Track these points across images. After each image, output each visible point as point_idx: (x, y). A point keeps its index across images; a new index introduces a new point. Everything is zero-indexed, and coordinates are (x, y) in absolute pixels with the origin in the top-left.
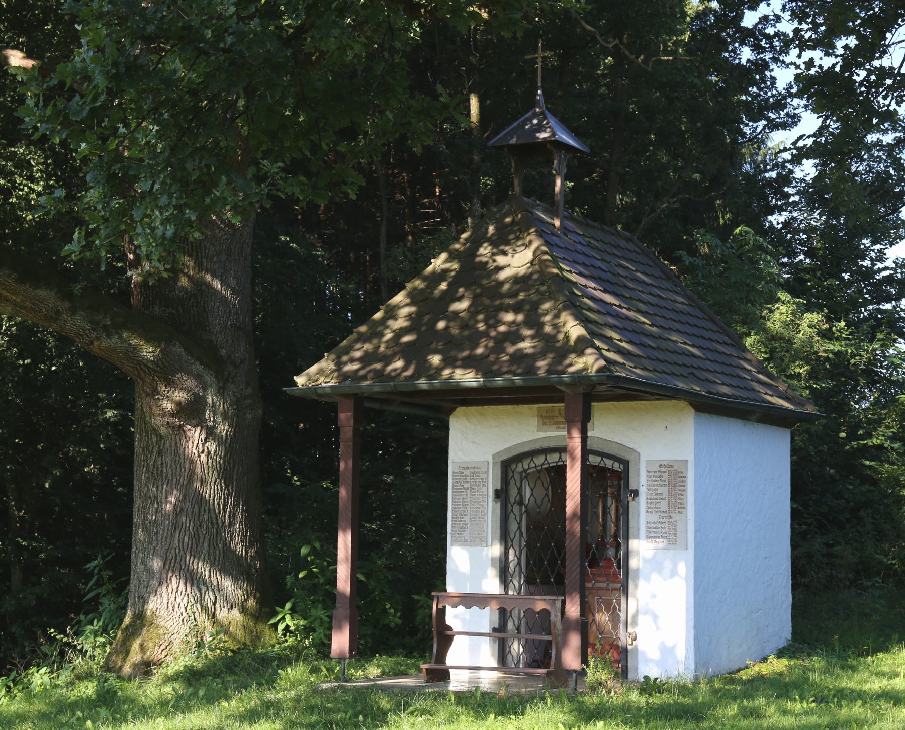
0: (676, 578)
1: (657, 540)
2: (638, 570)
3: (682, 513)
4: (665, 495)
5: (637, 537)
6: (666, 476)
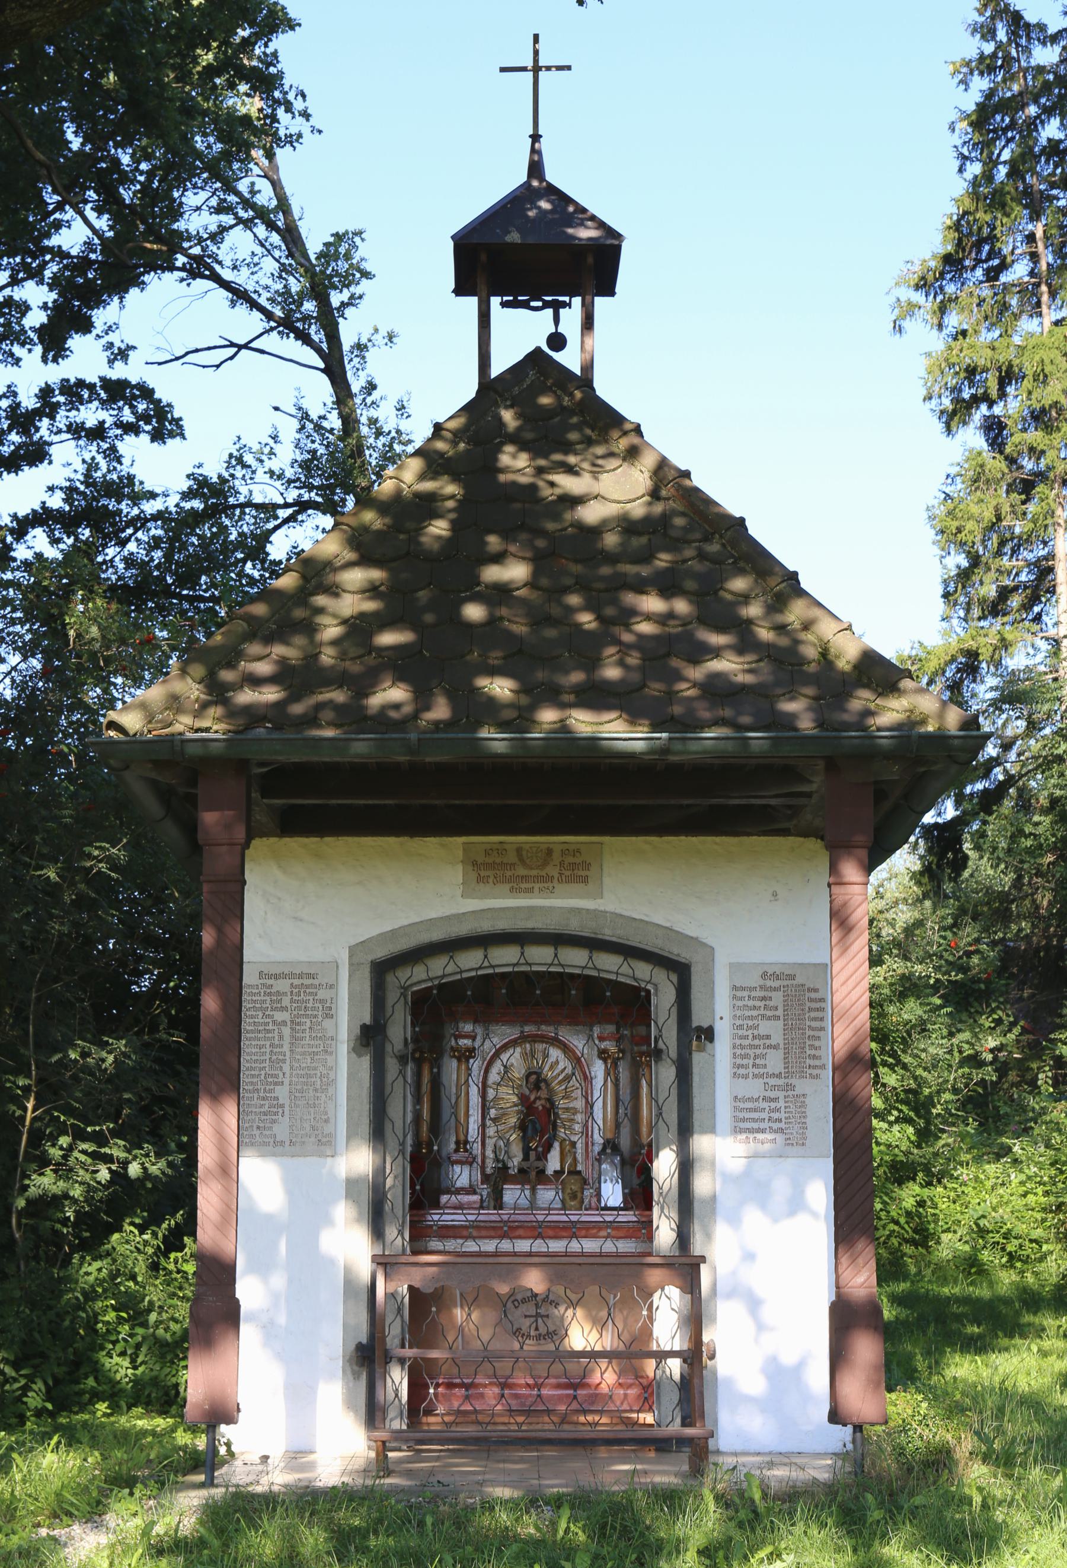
0: (802, 1218)
1: (760, 1136)
2: (714, 1198)
3: (817, 1076)
4: (777, 1038)
5: (712, 1130)
6: (777, 998)
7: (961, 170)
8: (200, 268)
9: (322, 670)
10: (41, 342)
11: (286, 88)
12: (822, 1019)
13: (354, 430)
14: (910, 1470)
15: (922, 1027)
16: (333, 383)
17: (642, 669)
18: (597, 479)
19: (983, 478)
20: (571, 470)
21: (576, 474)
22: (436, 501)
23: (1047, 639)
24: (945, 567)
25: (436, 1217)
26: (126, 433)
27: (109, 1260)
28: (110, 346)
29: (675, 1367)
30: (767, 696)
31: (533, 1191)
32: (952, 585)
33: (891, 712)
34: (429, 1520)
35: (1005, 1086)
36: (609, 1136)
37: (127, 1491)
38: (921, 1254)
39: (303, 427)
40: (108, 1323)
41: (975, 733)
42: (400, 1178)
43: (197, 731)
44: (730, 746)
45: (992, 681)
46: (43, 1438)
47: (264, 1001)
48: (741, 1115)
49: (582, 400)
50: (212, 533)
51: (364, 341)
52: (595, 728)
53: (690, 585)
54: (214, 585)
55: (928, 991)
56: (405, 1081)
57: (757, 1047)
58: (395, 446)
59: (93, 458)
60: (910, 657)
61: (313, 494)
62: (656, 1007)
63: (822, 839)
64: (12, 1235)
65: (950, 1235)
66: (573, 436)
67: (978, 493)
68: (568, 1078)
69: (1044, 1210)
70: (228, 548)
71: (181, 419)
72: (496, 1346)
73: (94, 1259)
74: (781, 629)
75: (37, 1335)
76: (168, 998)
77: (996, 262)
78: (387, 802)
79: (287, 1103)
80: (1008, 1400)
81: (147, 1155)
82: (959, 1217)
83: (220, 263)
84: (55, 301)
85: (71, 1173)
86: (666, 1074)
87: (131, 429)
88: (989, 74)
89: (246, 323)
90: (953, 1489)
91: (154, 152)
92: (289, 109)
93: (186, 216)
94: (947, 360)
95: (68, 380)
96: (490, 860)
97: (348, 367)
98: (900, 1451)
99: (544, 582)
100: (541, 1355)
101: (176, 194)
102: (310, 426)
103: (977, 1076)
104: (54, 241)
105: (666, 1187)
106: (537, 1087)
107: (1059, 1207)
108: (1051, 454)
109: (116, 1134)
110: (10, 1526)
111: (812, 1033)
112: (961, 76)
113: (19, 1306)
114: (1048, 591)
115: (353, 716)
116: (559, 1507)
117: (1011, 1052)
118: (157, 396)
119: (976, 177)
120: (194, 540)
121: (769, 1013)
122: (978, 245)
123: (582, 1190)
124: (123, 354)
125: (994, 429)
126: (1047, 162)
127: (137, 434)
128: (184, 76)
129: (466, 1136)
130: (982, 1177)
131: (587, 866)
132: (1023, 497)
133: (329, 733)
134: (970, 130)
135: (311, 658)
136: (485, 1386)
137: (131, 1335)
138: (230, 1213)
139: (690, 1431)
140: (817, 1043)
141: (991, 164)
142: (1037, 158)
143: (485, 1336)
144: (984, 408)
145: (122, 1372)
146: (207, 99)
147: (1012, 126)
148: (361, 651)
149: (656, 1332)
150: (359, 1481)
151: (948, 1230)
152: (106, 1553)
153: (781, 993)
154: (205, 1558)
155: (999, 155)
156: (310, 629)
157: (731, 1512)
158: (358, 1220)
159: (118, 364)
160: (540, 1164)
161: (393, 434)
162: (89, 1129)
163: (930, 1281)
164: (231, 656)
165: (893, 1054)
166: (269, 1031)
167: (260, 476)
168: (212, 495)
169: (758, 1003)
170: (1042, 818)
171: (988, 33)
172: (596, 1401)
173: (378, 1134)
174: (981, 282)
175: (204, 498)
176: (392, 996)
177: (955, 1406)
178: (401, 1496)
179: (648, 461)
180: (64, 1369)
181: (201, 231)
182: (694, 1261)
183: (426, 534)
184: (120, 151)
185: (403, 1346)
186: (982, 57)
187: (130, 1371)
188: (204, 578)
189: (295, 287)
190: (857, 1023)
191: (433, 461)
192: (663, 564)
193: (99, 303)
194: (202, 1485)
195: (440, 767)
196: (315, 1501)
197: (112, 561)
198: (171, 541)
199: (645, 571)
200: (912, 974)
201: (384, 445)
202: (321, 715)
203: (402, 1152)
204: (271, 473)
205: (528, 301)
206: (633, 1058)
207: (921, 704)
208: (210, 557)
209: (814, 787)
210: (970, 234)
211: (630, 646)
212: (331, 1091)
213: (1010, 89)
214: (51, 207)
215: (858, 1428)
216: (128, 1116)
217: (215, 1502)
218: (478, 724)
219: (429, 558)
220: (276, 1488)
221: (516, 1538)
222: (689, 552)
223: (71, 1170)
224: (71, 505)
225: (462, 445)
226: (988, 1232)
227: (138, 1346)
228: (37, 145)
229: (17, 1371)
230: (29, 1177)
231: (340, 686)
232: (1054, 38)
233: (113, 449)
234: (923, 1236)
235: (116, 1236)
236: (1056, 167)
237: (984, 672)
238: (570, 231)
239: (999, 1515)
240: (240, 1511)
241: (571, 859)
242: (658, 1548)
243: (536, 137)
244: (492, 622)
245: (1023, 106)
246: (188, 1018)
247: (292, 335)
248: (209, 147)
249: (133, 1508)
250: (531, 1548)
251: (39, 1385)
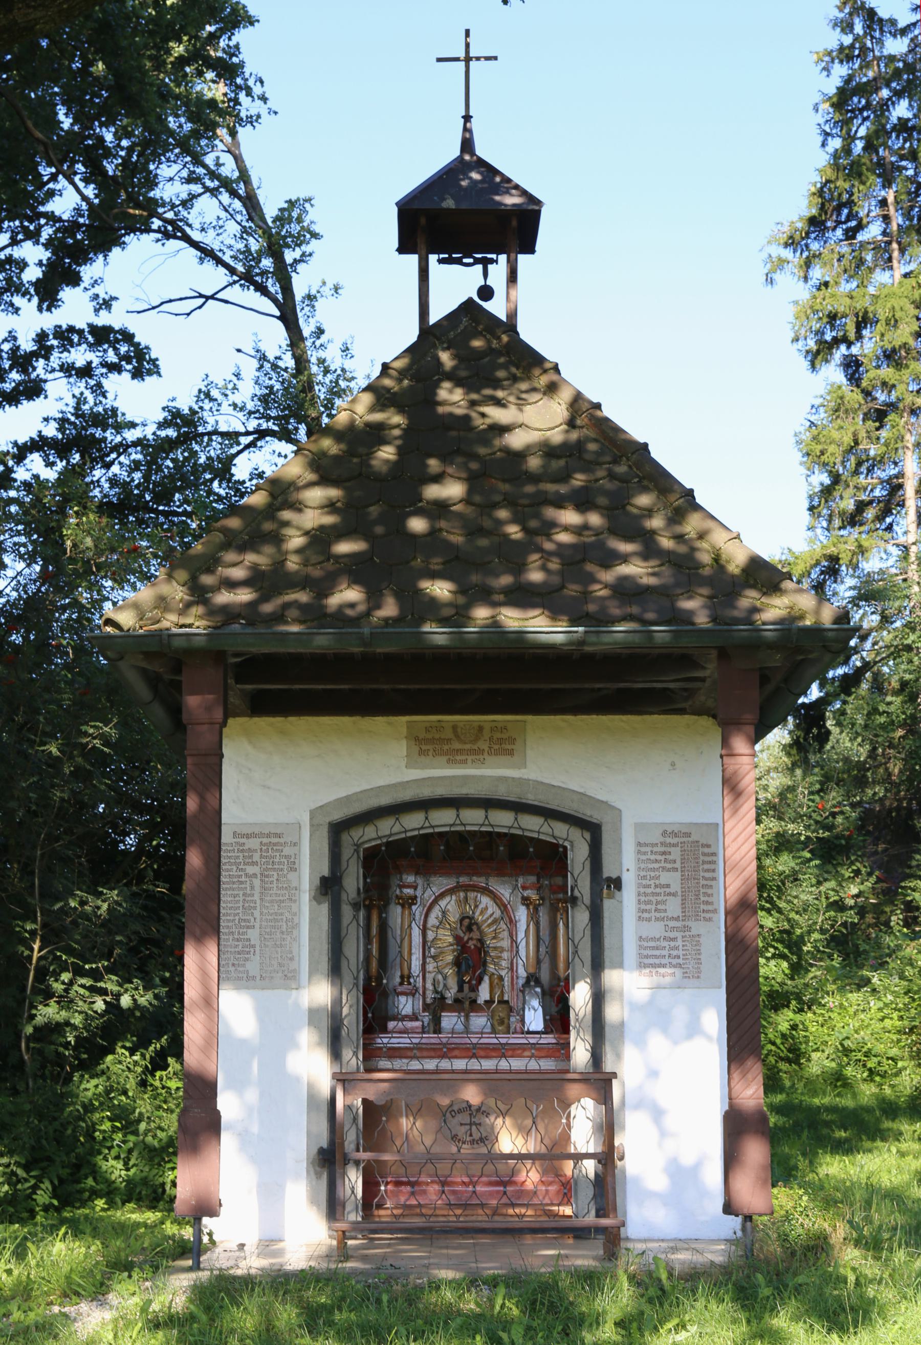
0: (698, 1043)
1: (662, 970)
2: (622, 1024)
3: (710, 919)
4: (676, 887)
5: (620, 965)
6: (676, 853)
7: (824, 145)
8: (175, 231)
9: (288, 574)
10: (37, 293)
11: (247, 75)
12: (714, 871)
13: (305, 369)
14: (793, 1254)
15: (794, 877)
16: (288, 328)
17: (561, 573)
18: (521, 410)
19: (843, 409)
20: (499, 403)
21: (504, 406)
22: (384, 429)
23: (898, 545)
24: (810, 484)
25: (385, 1041)
26: (110, 372)
27: (104, 1078)
28: (96, 296)
29: (590, 1167)
30: (668, 596)
31: (467, 1017)
32: (817, 499)
33: (774, 609)
34: (385, 1298)
35: (863, 927)
36: (531, 970)
37: (126, 1274)
38: (795, 1070)
39: (262, 366)
40: (105, 1131)
41: (846, 626)
42: (355, 1007)
43: (181, 627)
44: (637, 638)
45: (850, 582)
46: (53, 1229)
47: (238, 857)
48: (645, 952)
49: (508, 342)
50: (185, 458)
51: (313, 292)
52: (521, 623)
53: (602, 501)
54: (186, 501)
55: (800, 846)
56: (358, 924)
57: (658, 894)
58: (341, 382)
59: (82, 394)
60: (780, 561)
61: (270, 424)
62: (572, 861)
63: (714, 717)
64: (21, 1055)
65: (819, 1054)
66: (501, 374)
67: (839, 421)
68: (495, 921)
69: (899, 1032)
70: (197, 470)
71: (157, 359)
72: (436, 1149)
73: (92, 1077)
74: (679, 538)
75: (44, 1142)
76: (153, 855)
77: (853, 223)
78: (342, 687)
79: (258, 944)
80: (873, 1194)
81: (136, 989)
82: (826, 1038)
83: (190, 226)
84: (49, 259)
85: (73, 1004)
86: (581, 918)
87: (114, 368)
88: (848, 62)
89: (213, 277)
90: (831, 1269)
91: (133, 131)
92: (249, 93)
93: (160, 186)
94: (811, 307)
95: (60, 327)
96: (429, 736)
97: (300, 315)
98: (784, 1238)
99: (477, 499)
100: (478, 1157)
101: (152, 167)
102: (267, 366)
103: (841, 918)
104: (49, 207)
105: (581, 1014)
106: (469, 929)
107: (912, 1030)
108: (901, 388)
109: (109, 970)
110: (27, 1304)
111: (705, 882)
112: (823, 64)
113: (29, 1117)
114: (898, 505)
115: (315, 614)
116: (495, 1287)
117: (867, 898)
118: (136, 340)
119: (836, 150)
120: (169, 463)
121: (669, 866)
122: (838, 209)
123: (509, 1017)
124: (107, 304)
125: (852, 367)
126: (898, 137)
127: (120, 372)
128: (159, 65)
129: (410, 968)
130: (846, 1004)
131: (513, 741)
132: (877, 424)
133: (295, 628)
134: (831, 110)
135: (279, 564)
136: (427, 1184)
137: (124, 1142)
138: (212, 1038)
139: (605, 1222)
140: (709, 891)
141: (849, 139)
142: (888, 134)
143: (428, 1141)
144: (843, 348)
145: (117, 1173)
146: (178, 85)
147: (868, 106)
148: (321, 558)
149: (574, 1137)
150: (324, 1265)
151: (817, 1050)
152: (110, 1327)
153: (679, 849)
154: (196, 1331)
155: (856, 132)
156: (277, 539)
157: (641, 1291)
158: (319, 1044)
159: (103, 313)
160: (472, 995)
161: (339, 372)
162: (87, 967)
163: (802, 1094)
164: (210, 563)
165: (770, 900)
166: (242, 883)
167: (226, 408)
168: (184, 425)
169: (659, 857)
170: (894, 699)
171: (847, 27)
172: (522, 1196)
173: (335, 970)
174: (841, 240)
175: (178, 427)
176: (347, 852)
177: (830, 1198)
178: (360, 1278)
179: (565, 395)
180: (68, 1171)
181: (174, 199)
182: (607, 1077)
183: (375, 458)
184: (104, 129)
185: (358, 1150)
186: (842, 48)
187: (123, 1173)
188: (177, 495)
189: (254, 246)
190: (746, 874)
191: (381, 395)
192: (579, 483)
193: (86, 260)
194: (190, 1269)
195: (388, 657)
196: (287, 1282)
197: (98, 481)
198: (149, 464)
199: (563, 489)
200: (785, 831)
201: (331, 382)
202: (286, 613)
203: (356, 985)
204: (235, 406)
205: (461, 258)
206: (551, 904)
207: (792, 603)
208: (183, 478)
209: (707, 673)
210: (832, 199)
211: (551, 554)
212: (295, 932)
213: (865, 75)
214: (46, 179)
215: (748, 1218)
216: (119, 955)
217: (202, 1284)
218: (422, 620)
219: (378, 478)
220: (253, 1271)
221: (459, 1313)
222: (601, 473)
223: (72, 1001)
224: (63, 434)
225: (406, 382)
226: (851, 1051)
227: (130, 1151)
228: (36, 125)
229: (28, 1173)
230: (36, 1008)
231: (304, 588)
232: (904, 32)
233: (99, 385)
234: (796, 1055)
235: (110, 1058)
236: (905, 141)
237: (844, 574)
238: (497, 198)
239: (871, 1292)
240: (223, 1291)
241: (499, 735)
242: (581, 1321)
243: (467, 118)
244: (433, 532)
245: (877, 90)
246: (174, 871)
247: (252, 288)
248: (181, 126)
249: (132, 1289)
250: (472, 1324)
251: (47, 1185)
